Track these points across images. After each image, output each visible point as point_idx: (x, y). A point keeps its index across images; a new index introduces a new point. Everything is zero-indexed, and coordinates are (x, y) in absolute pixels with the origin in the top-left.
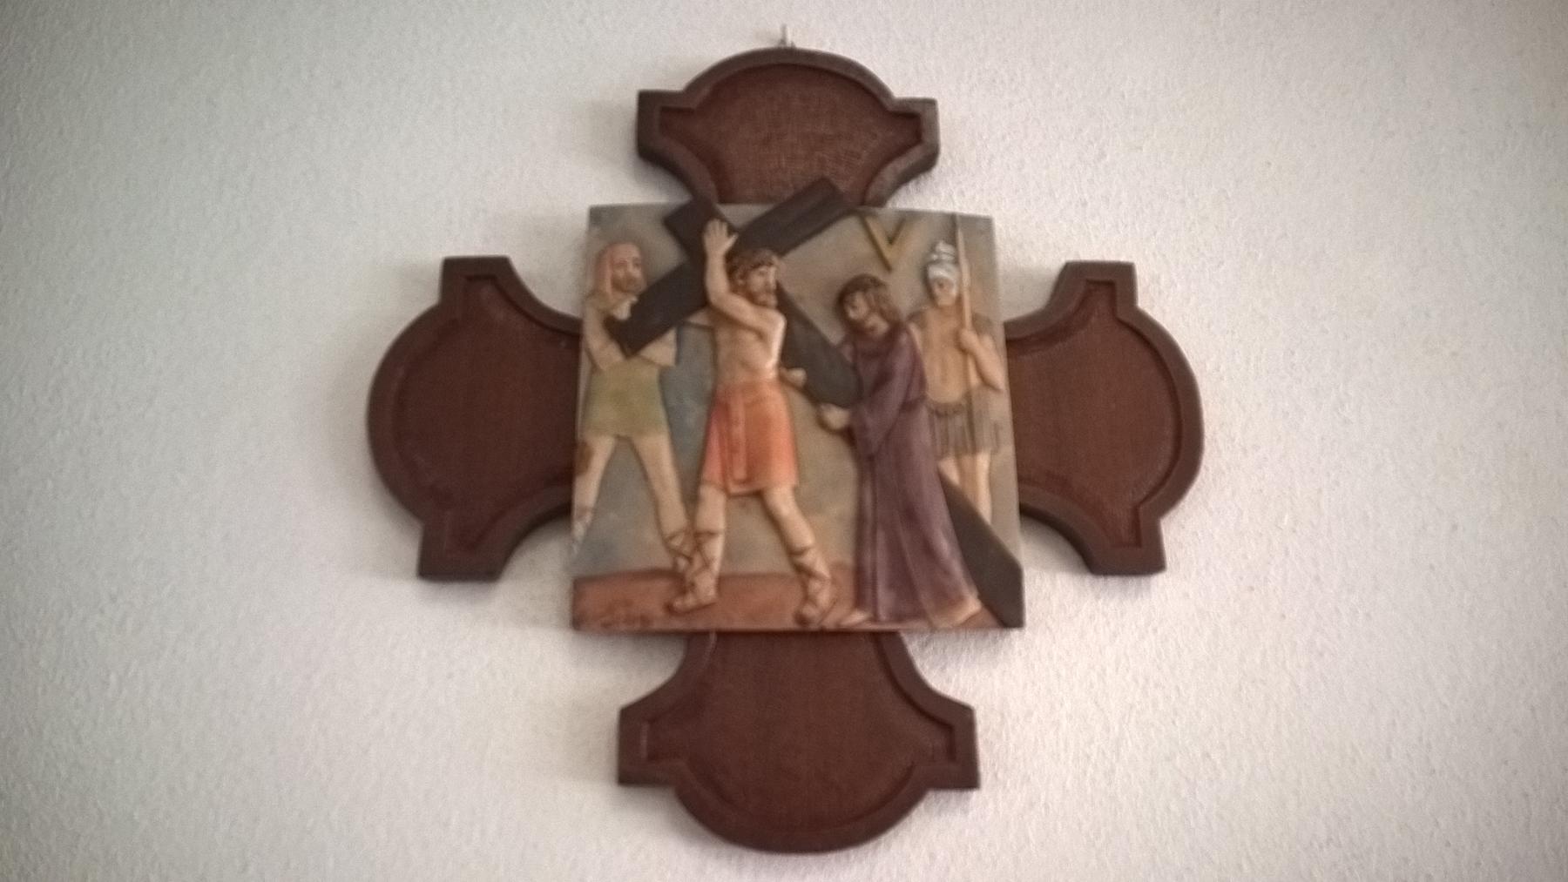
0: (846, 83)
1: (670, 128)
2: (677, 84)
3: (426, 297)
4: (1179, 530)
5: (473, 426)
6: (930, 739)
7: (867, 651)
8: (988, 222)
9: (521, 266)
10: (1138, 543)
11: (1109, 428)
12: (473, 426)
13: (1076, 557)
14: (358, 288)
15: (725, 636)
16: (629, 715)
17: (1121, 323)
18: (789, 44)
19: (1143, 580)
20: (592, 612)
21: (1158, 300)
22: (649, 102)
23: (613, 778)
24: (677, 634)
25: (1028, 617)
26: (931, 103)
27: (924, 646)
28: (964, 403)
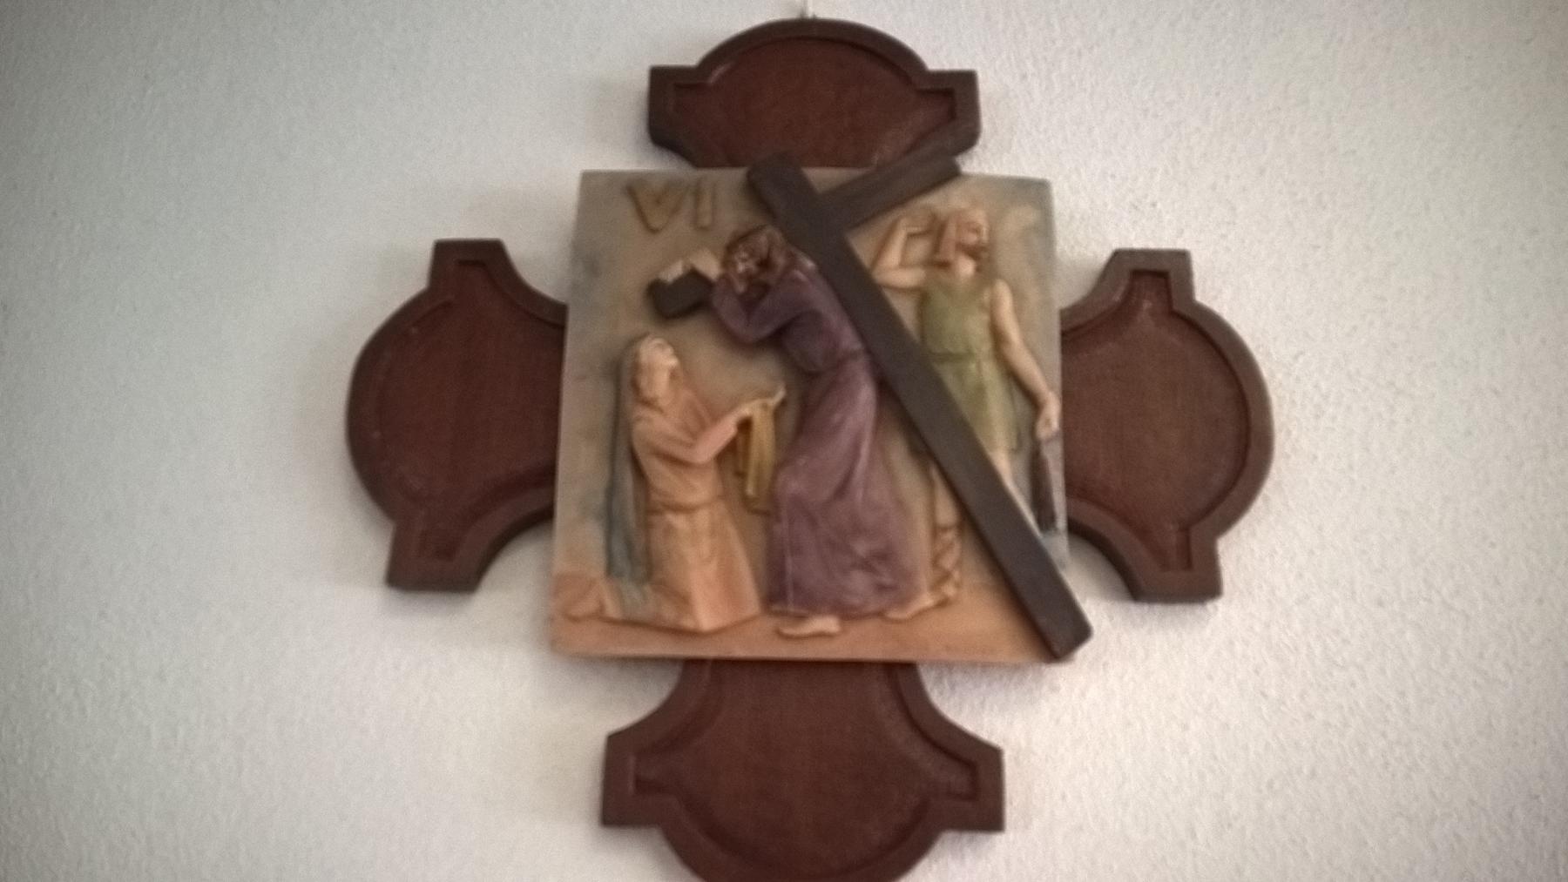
0: (870, 54)
1: (685, 106)
2: (692, 59)
3: (414, 282)
4: (1241, 550)
5: (455, 424)
6: (955, 778)
7: (878, 690)
8: (1181, 259)
9: (517, 251)
10: (1188, 565)
11: (1159, 442)
12: (455, 424)
13: (1117, 580)
14: (361, 274)
15: (721, 664)
16: (617, 743)
17: (1174, 315)
18: (810, 15)
19: (1198, 610)
20: (565, 634)
21: (1213, 291)
22: (664, 81)
23: (596, 819)
24: (673, 661)
25: (1011, 813)
26: (1182, 257)
27: (939, 679)
28: (688, 623)
